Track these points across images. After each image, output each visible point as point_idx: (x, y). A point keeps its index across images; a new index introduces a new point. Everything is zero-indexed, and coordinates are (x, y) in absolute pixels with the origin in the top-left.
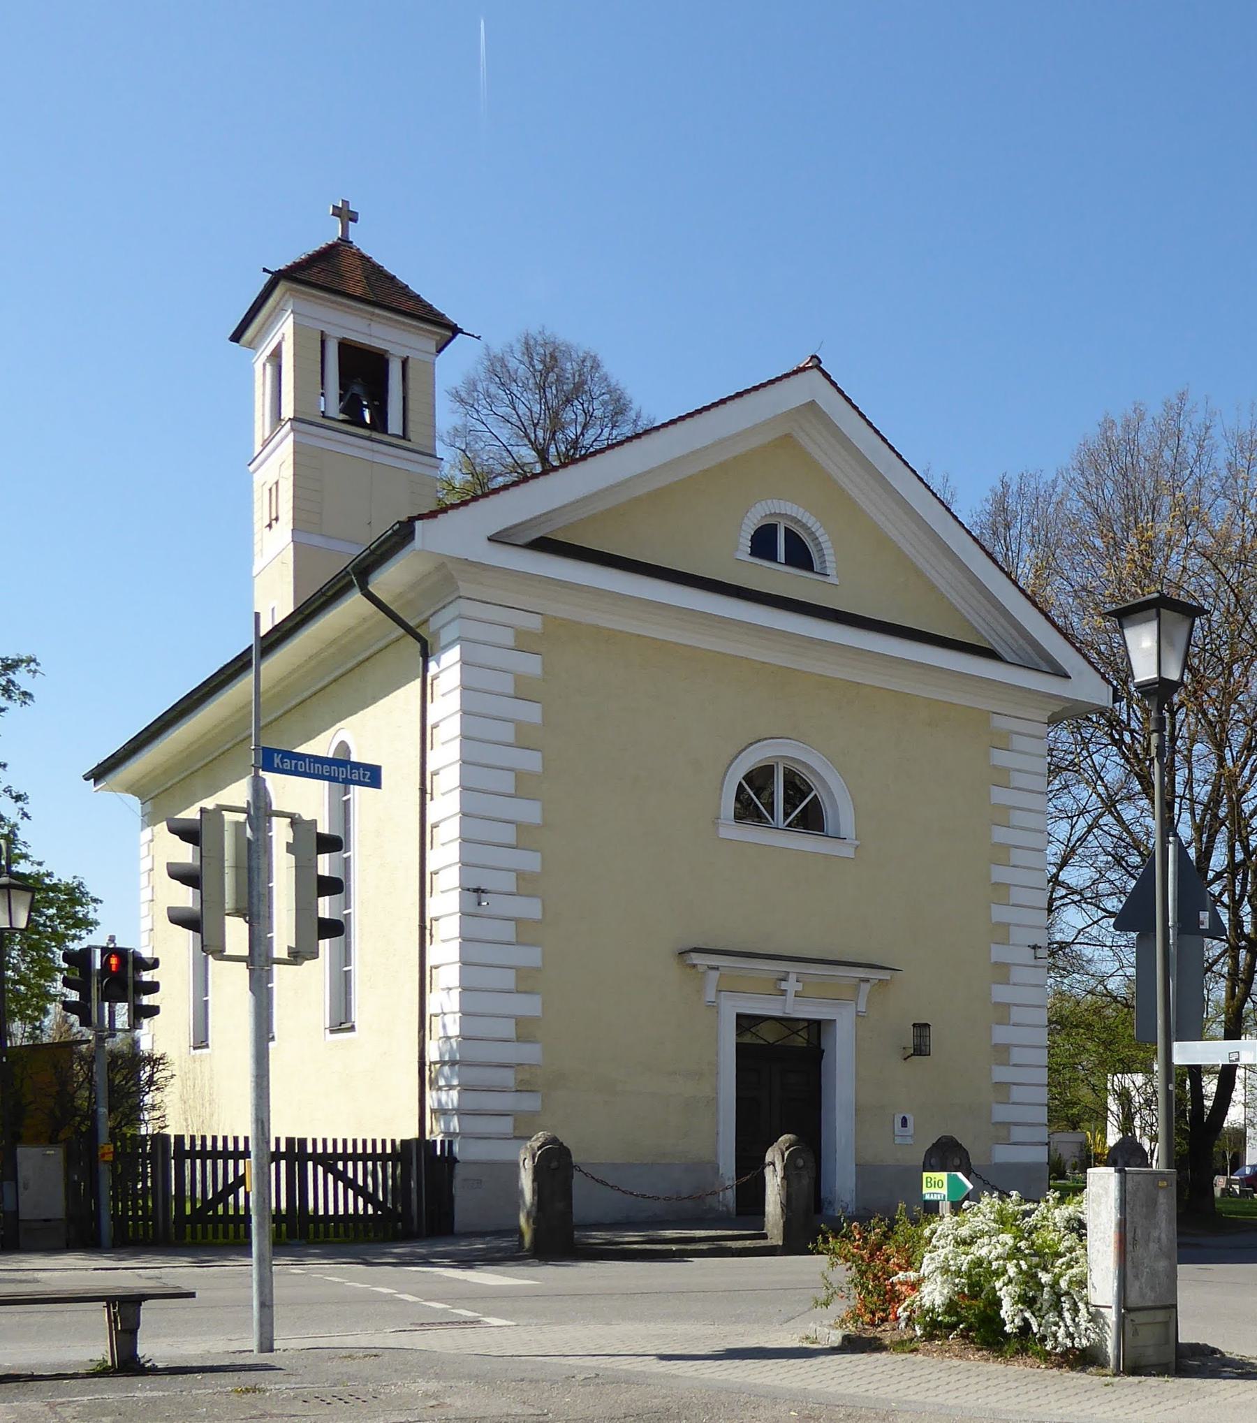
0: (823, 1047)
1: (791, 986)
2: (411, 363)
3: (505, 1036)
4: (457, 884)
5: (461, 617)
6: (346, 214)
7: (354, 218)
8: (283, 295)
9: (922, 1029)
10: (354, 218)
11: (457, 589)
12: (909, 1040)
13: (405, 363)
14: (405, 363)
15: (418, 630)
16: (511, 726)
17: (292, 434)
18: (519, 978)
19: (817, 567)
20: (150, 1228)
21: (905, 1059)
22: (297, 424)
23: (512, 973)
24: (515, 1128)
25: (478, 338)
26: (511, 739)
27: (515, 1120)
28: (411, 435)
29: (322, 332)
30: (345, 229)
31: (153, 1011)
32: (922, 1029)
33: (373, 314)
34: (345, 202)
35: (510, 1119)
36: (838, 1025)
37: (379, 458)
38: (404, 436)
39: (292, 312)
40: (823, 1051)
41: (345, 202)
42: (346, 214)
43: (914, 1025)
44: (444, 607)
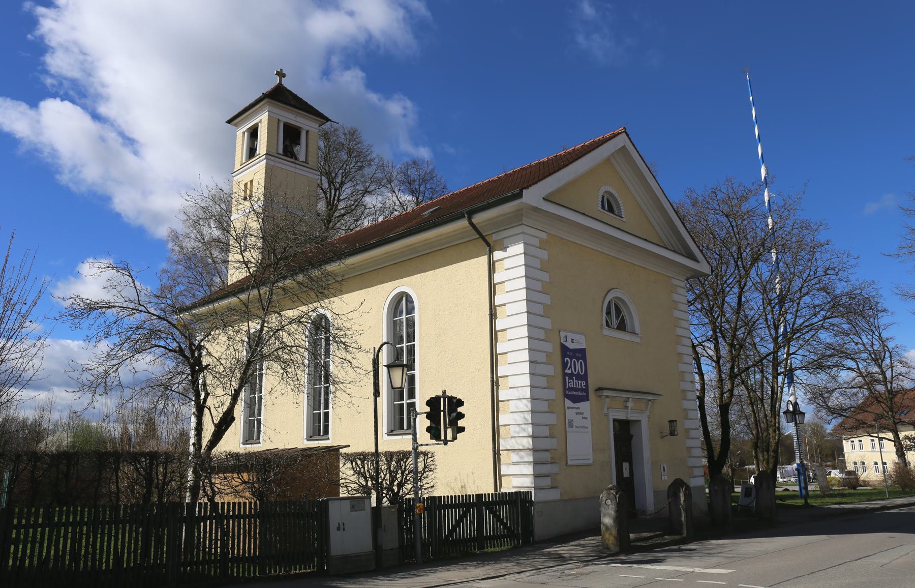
0: (632, 432)
1: (630, 404)
2: (310, 133)
3: (544, 435)
4: (527, 359)
5: (523, 233)
6: (281, 74)
7: (284, 76)
8: (265, 103)
9: (672, 422)
10: (284, 76)
11: (522, 220)
12: (667, 430)
13: (307, 132)
14: (307, 132)
15: (486, 238)
16: (540, 283)
17: (265, 160)
18: (549, 405)
19: (616, 212)
20: (57, 513)
21: (662, 438)
22: (267, 156)
23: (546, 403)
24: (552, 482)
25: (338, 123)
26: (540, 289)
27: (551, 479)
28: (309, 162)
29: (278, 119)
30: (280, 80)
31: (462, 429)
32: (672, 422)
33: (299, 113)
34: (281, 70)
35: (549, 478)
36: (642, 422)
37: (298, 171)
38: (306, 162)
39: (268, 111)
40: (632, 436)
41: (281, 70)
42: (281, 74)
43: (669, 421)
44: (505, 229)
